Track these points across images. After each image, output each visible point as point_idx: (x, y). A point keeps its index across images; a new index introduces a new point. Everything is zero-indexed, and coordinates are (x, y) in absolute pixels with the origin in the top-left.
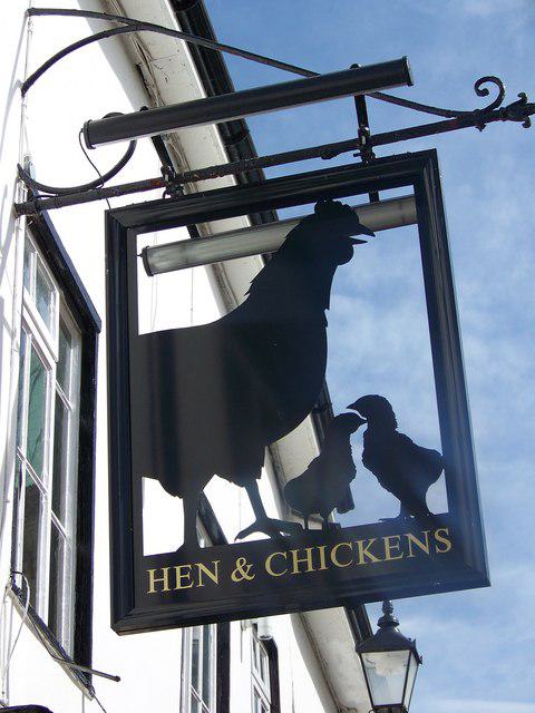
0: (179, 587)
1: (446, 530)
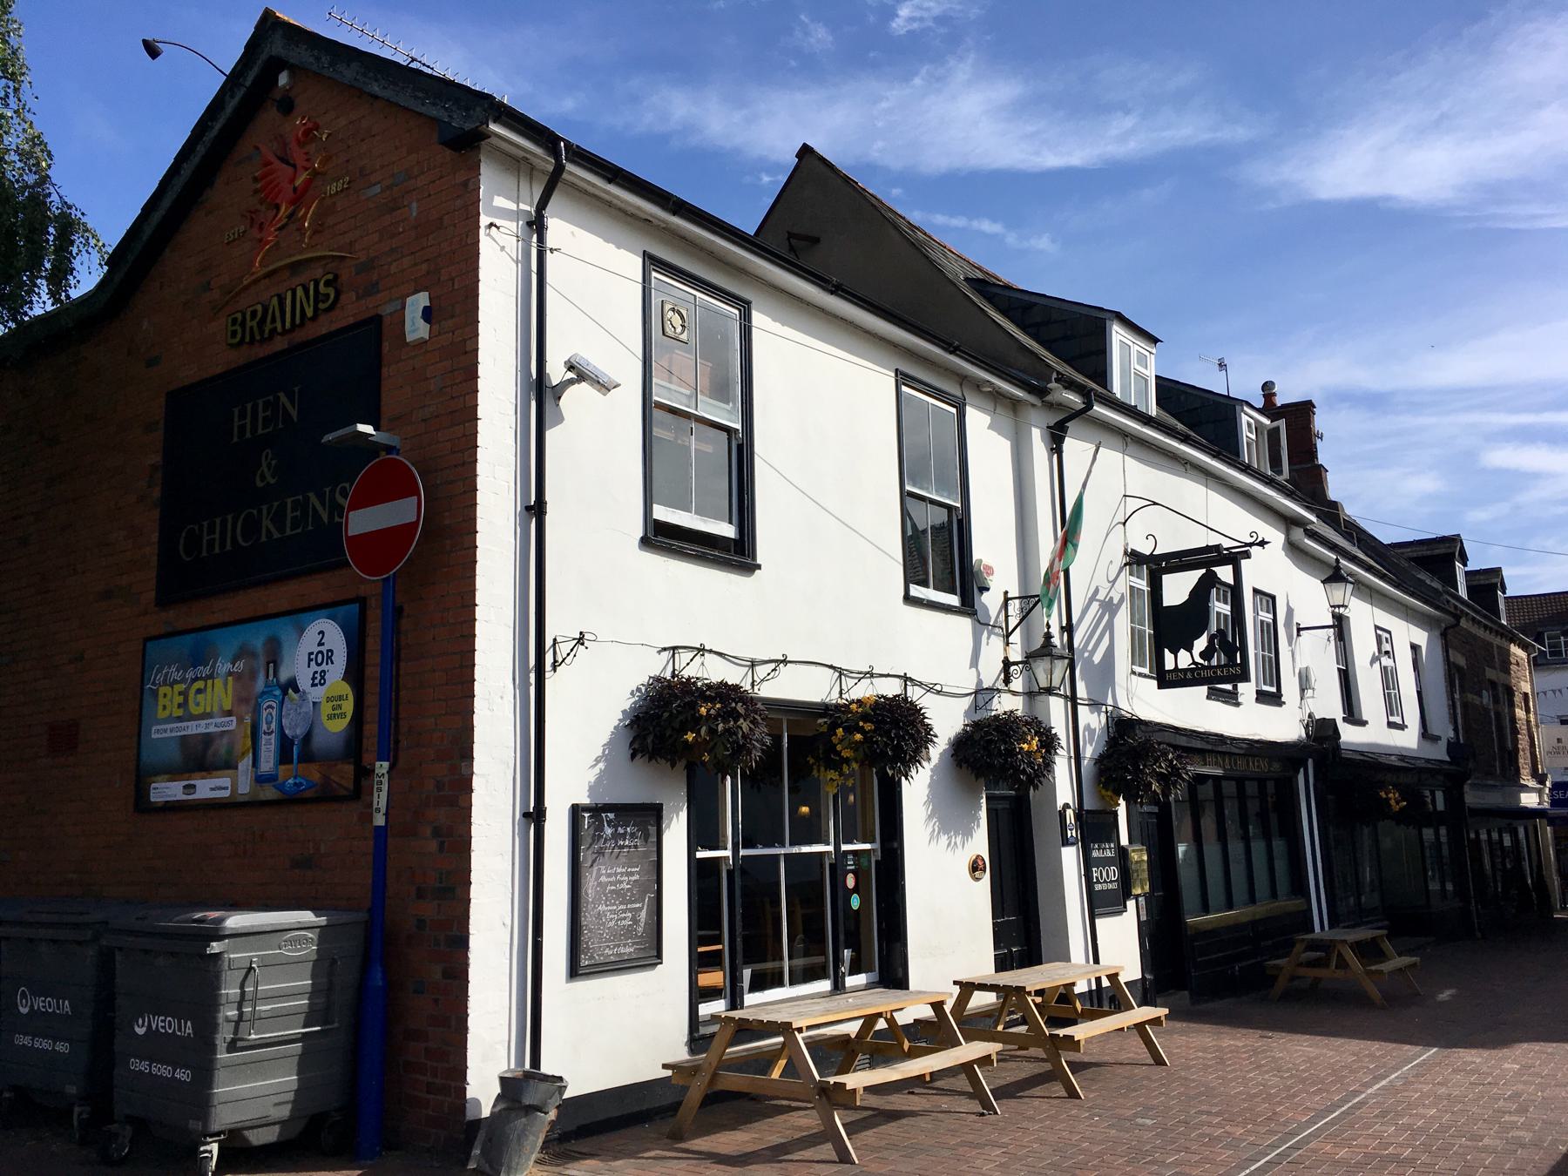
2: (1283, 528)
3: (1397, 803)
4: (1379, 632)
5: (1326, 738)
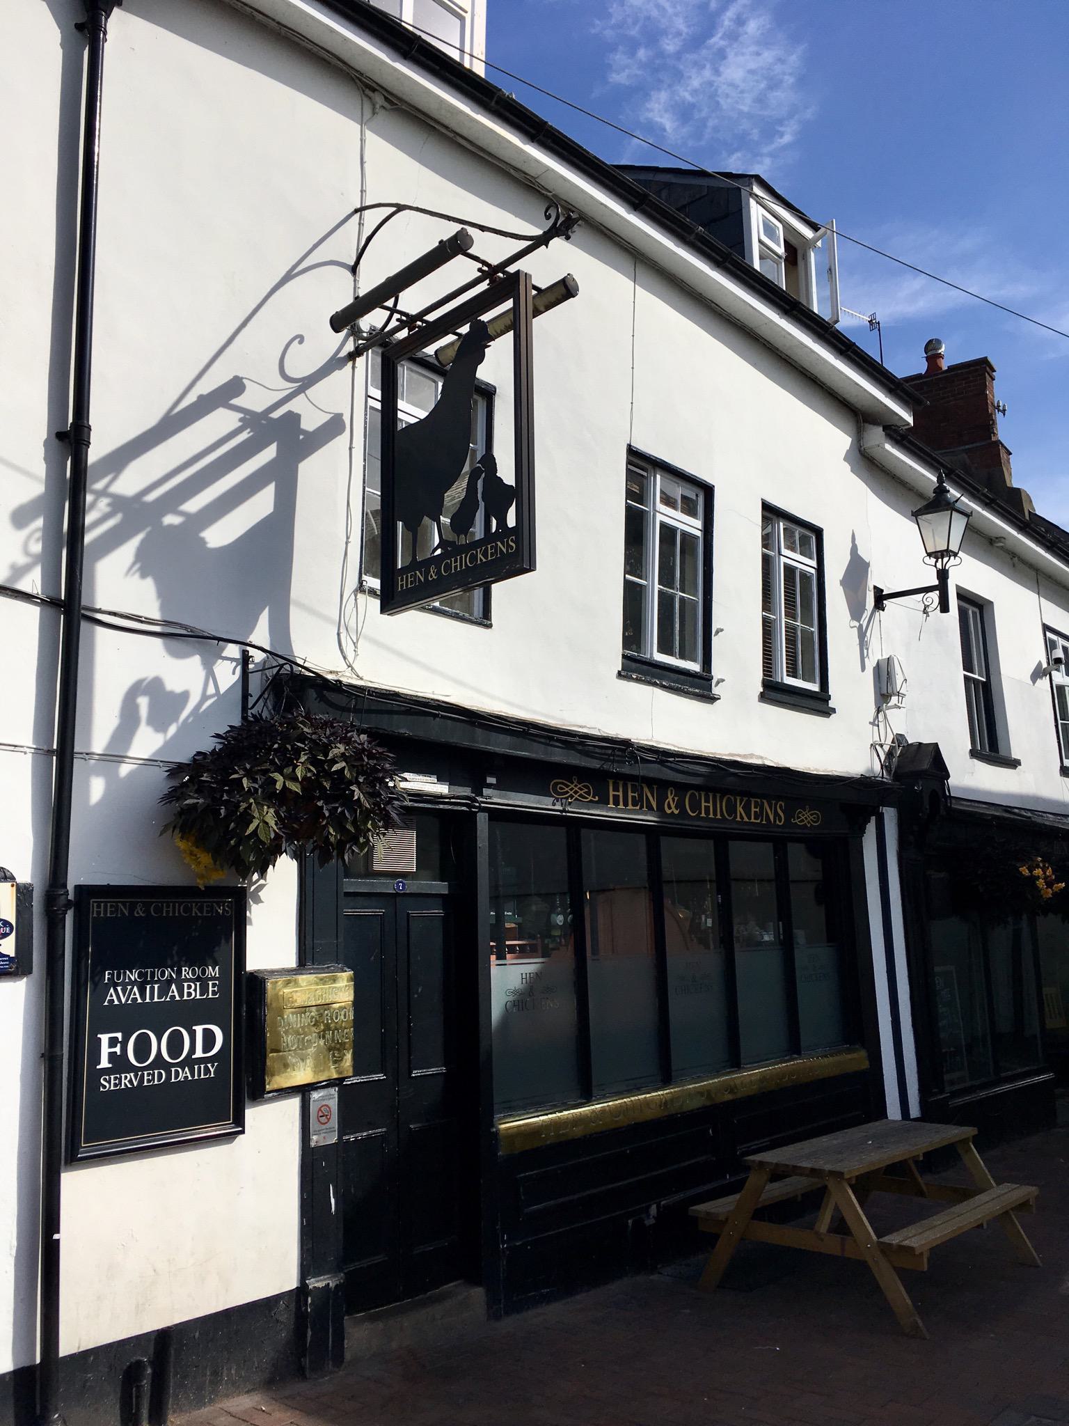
0: (108, 915)
1: (102, 1089)
2: (851, 426)
3: (1049, 884)
4: (1049, 635)
5: (919, 775)
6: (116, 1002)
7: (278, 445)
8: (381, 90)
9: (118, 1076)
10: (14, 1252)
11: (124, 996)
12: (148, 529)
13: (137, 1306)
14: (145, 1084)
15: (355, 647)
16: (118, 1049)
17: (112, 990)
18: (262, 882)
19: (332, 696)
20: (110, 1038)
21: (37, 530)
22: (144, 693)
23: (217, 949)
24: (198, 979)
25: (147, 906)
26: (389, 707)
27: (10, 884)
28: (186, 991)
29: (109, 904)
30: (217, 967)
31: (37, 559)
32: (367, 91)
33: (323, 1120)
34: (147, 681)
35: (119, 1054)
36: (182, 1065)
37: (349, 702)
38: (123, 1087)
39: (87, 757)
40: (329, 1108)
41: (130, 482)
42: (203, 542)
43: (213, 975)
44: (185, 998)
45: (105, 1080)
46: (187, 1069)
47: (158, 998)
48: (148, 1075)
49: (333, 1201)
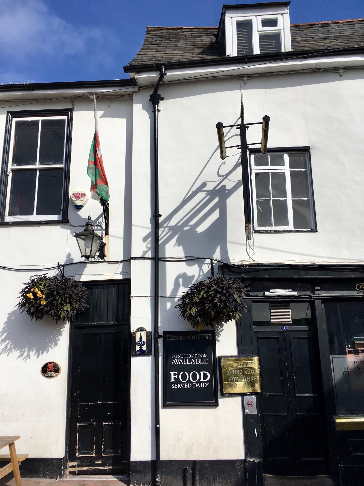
1: (172, 387)
6: (175, 363)
7: (219, 197)
8: (245, 76)
9: (177, 384)
10: (150, 428)
11: (178, 362)
12: (180, 233)
13: (187, 452)
14: (185, 387)
15: (253, 251)
16: (176, 377)
17: (174, 360)
18: (221, 329)
19: (232, 269)
20: (174, 373)
21: (149, 241)
22: (181, 278)
23: (207, 349)
24: (201, 358)
25: (183, 337)
26: (258, 269)
27: (144, 332)
28: (197, 361)
29: (172, 337)
30: (207, 355)
31: (150, 248)
32: (241, 79)
33: (250, 406)
34: (181, 274)
35: (177, 378)
36: (197, 383)
37: (241, 270)
38: (178, 387)
39: (165, 297)
40: (253, 403)
41: (173, 222)
42: (196, 232)
43: (206, 357)
44: (197, 363)
45: (173, 385)
46: (198, 384)
47: (202, 363)
48: (186, 385)
49: (256, 433)
